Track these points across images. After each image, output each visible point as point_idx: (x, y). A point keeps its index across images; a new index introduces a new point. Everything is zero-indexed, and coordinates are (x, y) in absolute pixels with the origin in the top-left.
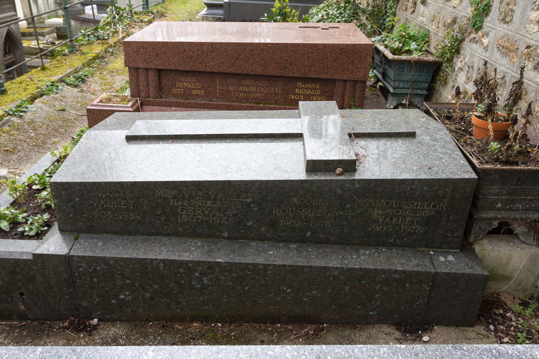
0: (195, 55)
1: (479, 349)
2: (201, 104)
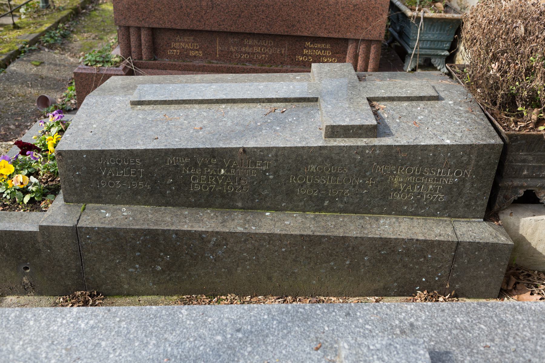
0: (193, 11)
1: (503, 305)
2: (200, 67)
